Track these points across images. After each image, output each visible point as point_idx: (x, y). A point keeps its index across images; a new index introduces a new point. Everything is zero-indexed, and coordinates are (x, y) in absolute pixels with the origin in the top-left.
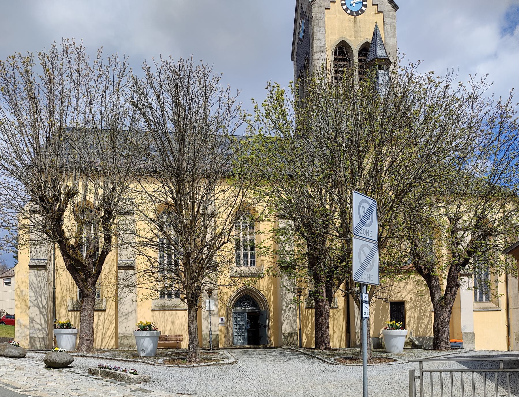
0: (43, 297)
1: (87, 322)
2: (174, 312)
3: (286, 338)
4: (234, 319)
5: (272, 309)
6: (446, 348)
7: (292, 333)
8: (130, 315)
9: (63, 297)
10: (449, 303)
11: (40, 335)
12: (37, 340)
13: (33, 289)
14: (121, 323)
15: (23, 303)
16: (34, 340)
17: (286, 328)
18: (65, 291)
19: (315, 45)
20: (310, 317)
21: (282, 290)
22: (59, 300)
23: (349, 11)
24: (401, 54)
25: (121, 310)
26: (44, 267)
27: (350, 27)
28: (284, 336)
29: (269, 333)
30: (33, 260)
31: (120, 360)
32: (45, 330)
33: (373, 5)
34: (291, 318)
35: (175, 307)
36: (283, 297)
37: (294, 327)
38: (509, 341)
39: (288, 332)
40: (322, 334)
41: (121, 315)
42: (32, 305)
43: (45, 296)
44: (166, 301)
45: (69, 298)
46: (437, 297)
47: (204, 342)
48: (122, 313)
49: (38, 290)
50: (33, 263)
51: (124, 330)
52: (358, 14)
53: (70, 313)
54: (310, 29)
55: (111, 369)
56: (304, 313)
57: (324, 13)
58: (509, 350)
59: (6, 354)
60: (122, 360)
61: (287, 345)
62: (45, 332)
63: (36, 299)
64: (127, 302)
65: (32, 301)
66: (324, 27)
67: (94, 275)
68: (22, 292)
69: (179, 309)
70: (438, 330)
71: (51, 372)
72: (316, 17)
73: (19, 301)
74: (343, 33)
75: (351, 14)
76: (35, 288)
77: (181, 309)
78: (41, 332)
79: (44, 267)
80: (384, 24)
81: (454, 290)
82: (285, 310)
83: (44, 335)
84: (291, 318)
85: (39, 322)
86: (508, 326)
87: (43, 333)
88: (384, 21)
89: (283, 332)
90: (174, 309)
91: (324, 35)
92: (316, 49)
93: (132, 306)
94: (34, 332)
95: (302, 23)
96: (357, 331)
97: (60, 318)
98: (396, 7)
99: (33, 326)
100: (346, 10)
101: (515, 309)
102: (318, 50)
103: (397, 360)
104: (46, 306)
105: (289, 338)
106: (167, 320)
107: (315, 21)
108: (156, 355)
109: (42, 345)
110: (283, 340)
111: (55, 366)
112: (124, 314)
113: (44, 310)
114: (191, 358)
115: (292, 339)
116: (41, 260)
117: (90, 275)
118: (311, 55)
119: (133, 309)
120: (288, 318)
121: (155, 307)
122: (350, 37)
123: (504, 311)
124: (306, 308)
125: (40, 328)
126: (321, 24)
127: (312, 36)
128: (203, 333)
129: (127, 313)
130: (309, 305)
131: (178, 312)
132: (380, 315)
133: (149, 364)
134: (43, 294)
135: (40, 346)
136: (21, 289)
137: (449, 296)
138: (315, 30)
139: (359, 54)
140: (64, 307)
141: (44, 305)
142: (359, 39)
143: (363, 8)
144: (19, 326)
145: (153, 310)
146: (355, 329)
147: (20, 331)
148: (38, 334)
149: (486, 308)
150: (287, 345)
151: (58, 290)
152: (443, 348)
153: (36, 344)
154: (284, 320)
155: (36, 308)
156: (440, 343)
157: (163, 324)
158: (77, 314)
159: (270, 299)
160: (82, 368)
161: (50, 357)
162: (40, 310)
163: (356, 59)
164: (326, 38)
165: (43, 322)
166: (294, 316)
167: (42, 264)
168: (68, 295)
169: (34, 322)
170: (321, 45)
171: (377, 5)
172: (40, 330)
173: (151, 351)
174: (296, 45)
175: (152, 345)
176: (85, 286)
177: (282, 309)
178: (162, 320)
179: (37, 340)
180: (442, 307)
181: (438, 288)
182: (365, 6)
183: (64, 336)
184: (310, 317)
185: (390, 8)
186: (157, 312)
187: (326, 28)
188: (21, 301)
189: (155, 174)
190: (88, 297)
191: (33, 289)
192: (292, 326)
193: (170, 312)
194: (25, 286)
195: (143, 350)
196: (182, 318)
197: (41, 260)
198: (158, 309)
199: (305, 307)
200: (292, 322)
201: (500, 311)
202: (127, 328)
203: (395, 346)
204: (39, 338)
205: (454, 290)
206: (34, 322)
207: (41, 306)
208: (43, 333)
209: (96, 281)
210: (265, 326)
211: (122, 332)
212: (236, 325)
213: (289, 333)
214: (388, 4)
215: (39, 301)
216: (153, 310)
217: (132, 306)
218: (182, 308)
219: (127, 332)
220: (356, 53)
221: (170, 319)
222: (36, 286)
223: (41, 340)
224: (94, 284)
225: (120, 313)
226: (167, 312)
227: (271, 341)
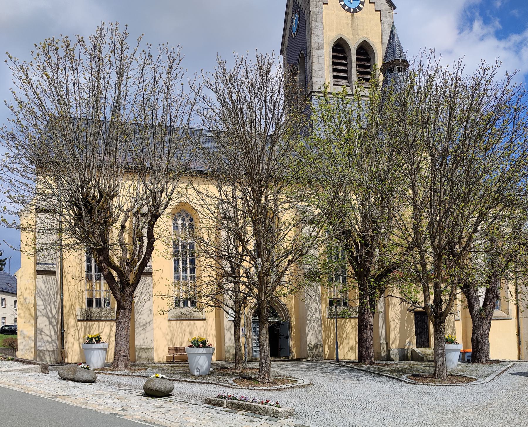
0: (53, 306)
1: (124, 336)
2: (192, 322)
3: (311, 349)
4: (253, 330)
5: (293, 319)
6: (486, 361)
7: (318, 345)
8: (148, 325)
9: (72, 305)
10: (489, 315)
11: (50, 347)
12: (47, 353)
13: (42, 297)
14: (138, 334)
15: (27, 312)
16: (44, 354)
17: (311, 339)
18: (73, 299)
19: (313, 41)
20: (332, 327)
21: (307, 299)
22: (68, 308)
23: (346, 8)
24: (499, 62)
25: (138, 320)
26: (54, 273)
27: (348, 24)
28: (309, 348)
29: (291, 343)
30: (41, 264)
31: (182, 381)
32: (55, 343)
33: (370, 3)
34: (316, 329)
35: (194, 317)
36: (308, 306)
37: (320, 338)
38: (519, 350)
39: (313, 343)
40: (367, 349)
41: (138, 326)
42: (40, 314)
43: (54, 305)
44: (182, 310)
45: (78, 307)
46: (476, 309)
47: (227, 355)
48: (139, 324)
49: (47, 298)
50: (40, 268)
51: (142, 342)
52: (355, 11)
53: (79, 323)
54: (307, 23)
55: (237, 400)
56: (326, 323)
57: (322, 8)
58: (519, 359)
59: (77, 379)
60: (184, 381)
61: (313, 357)
62: (55, 345)
63: (45, 308)
64: (144, 312)
65: (41, 310)
66: (322, 22)
67: (132, 284)
68: (25, 299)
69: (197, 318)
70: (478, 342)
71: (155, 401)
72: (314, 12)
73: (23, 310)
74: (341, 29)
75: (349, 10)
76: (43, 296)
77: (199, 318)
78: (51, 345)
79: (54, 273)
80: (381, 23)
81: (493, 301)
82: (310, 320)
83: (54, 348)
84: (316, 329)
85: (49, 334)
86: (519, 335)
87: (53, 346)
88: (381, 20)
89: (308, 343)
90: (192, 318)
91: (322, 30)
92: (314, 45)
93: (150, 316)
94: (43, 345)
95: (295, 17)
96: (381, 342)
97: (68, 328)
98: (393, 6)
99: (42, 338)
100: (344, 6)
101: (525, 317)
102: (316, 46)
103: (476, 380)
104: (56, 316)
105: (314, 350)
106: (185, 330)
107: (313, 16)
108: (210, 374)
109: (52, 359)
110: (309, 352)
111: (158, 395)
112: (141, 324)
113: (53, 320)
114: (263, 378)
115: (318, 350)
116: (50, 264)
117: (128, 285)
118: (308, 51)
119: (151, 319)
120: (312, 329)
121: (172, 316)
122: (348, 34)
123: (514, 320)
124: (328, 318)
125: (50, 340)
126: (319, 19)
127: (310, 30)
128: (226, 345)
129: (144, 323)
130: (331, 315)
131: (196, 322)
132: (406, 325)
133: (222, 385)
134: (52, 303)
135: (50, 361)
136: (25, 297)
137: (489, 307)
138: (313, 25)
139: (358, 53)
140: (72, 316)
141: (54, 314)
142: (357, 37)
143: (361, 6)
144: (22, 337)
145: (169, 320)
146: (380, 340)
147: (24, 343)
148: (48, 347)
149: (498, 317)
150: (313, 357)
151: (66, 297)
152: (484, 361)
153: (45, 358)
154: (309, 331)
155: (45, 318)
156: (480, 356)
157: (181, 335)
158: (87, 324)
159: (292, 308)
160: (181, 395)
161: (154, 385)
162: (49, 321)
163: (354, 57)
164: (324, 35)
165: (53, 333)
166: (319, 326)
167: (52, 269)
168: (77, 304)
169: (43, 333)
170: (319, 41)
171: (374, 3)
172: (50, 343)
173: (206, 369)
174: (287, 38)
175: (207, 363)
176: (122, 297)
177: (307, 319)
178: (179, 331)
179: (47, 353)
180: (482, 318)
181: (477, 299)
182: (363, 3)
183: (95, 351)
184: (332, 327)
185: (387, 7)
186: (174, 323)
187: (324, 23)
188: (24, 310)
189: (219, 177)
190: (124, 308)
191: (42, 297)
192: (317, 337)
193: (188, 322)
194: (29, 294)
195: (198, 368)
196: (200, 328)
197: (50, 264)
198: (174, 319)
199: (327, 316)
200: (318, 333)
201: (511, 319)
202: (146, 340)
203: (451, 361)
204: (49, 351)
205: (493, 301)
206: (43, 333)
207: (51, 316)
208: (53, 346)
209: (133, 292)
210: (287, 337)
211: (139, 344)
212: (255, 335)
213: (314, 345)
214: (385, 3)
215: (48, 310)
216: (169, 320)
217: (150, 316)
218: (201, 318)
219: (145, 344)
220: (353, 51)
221: (188, 330)
222: (45, 294)
223: (51, 353)
224: (131, 295)
225: (137, 323)
226: (184, 322)
227: (292, 352)
